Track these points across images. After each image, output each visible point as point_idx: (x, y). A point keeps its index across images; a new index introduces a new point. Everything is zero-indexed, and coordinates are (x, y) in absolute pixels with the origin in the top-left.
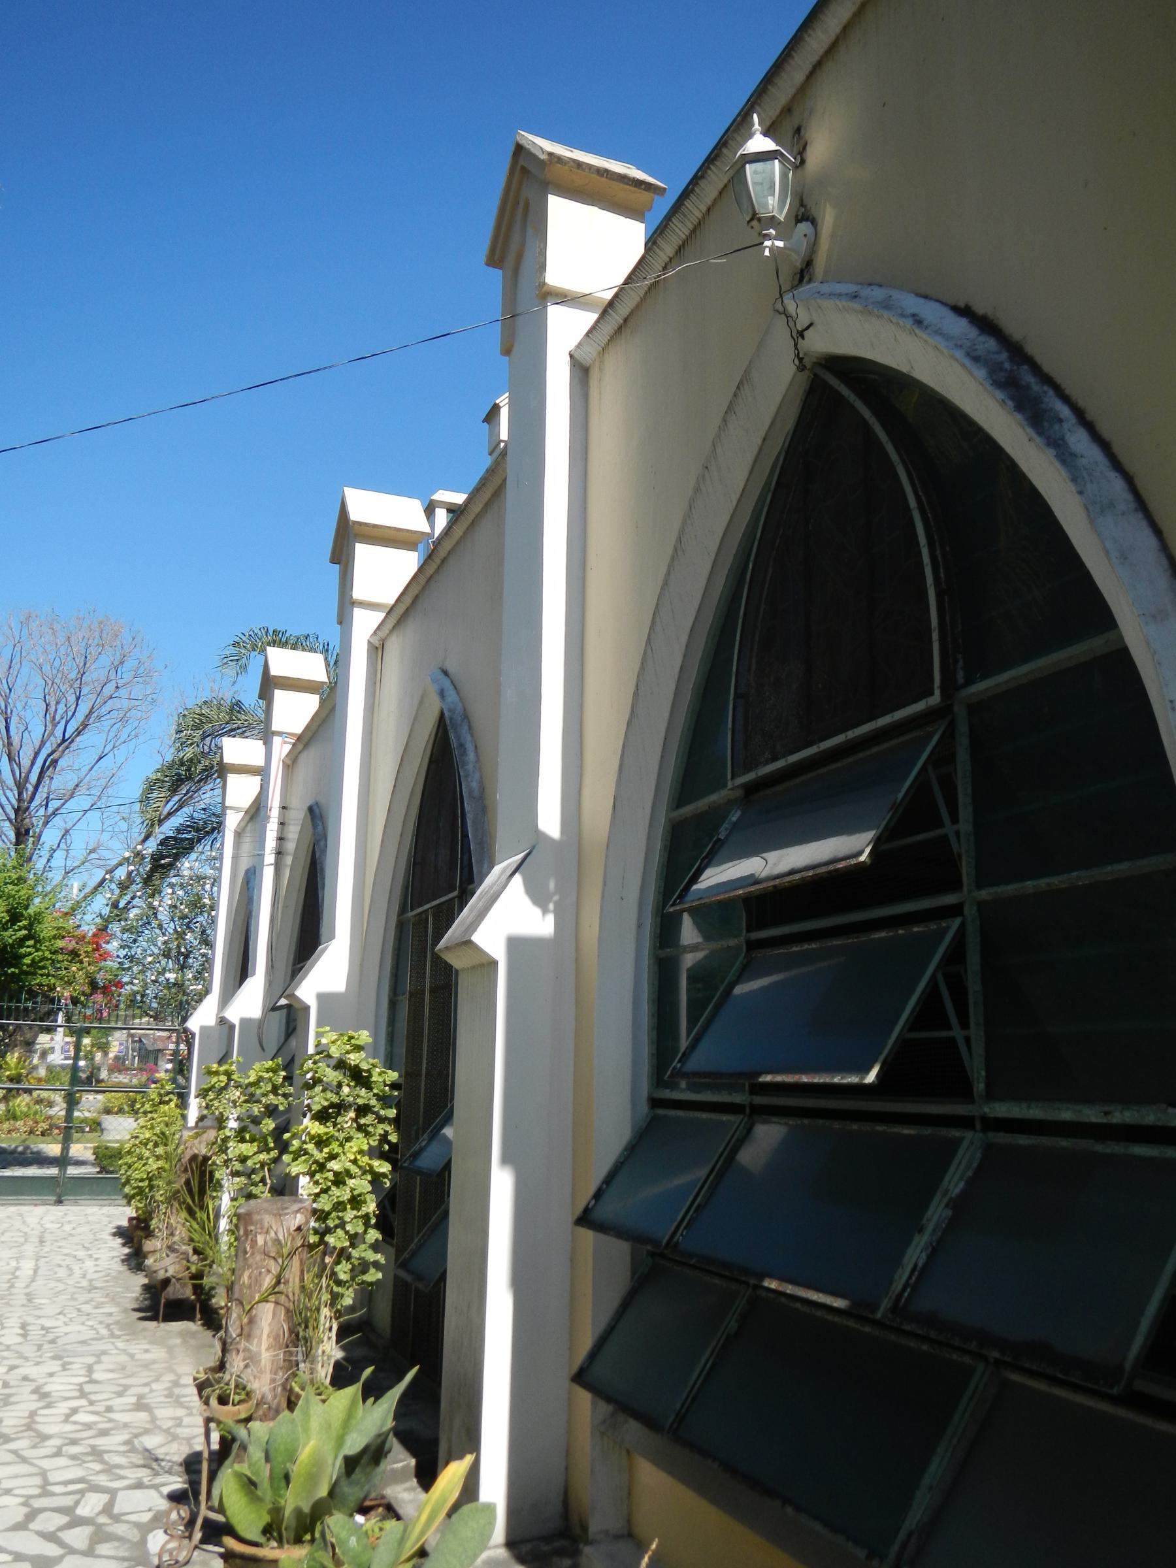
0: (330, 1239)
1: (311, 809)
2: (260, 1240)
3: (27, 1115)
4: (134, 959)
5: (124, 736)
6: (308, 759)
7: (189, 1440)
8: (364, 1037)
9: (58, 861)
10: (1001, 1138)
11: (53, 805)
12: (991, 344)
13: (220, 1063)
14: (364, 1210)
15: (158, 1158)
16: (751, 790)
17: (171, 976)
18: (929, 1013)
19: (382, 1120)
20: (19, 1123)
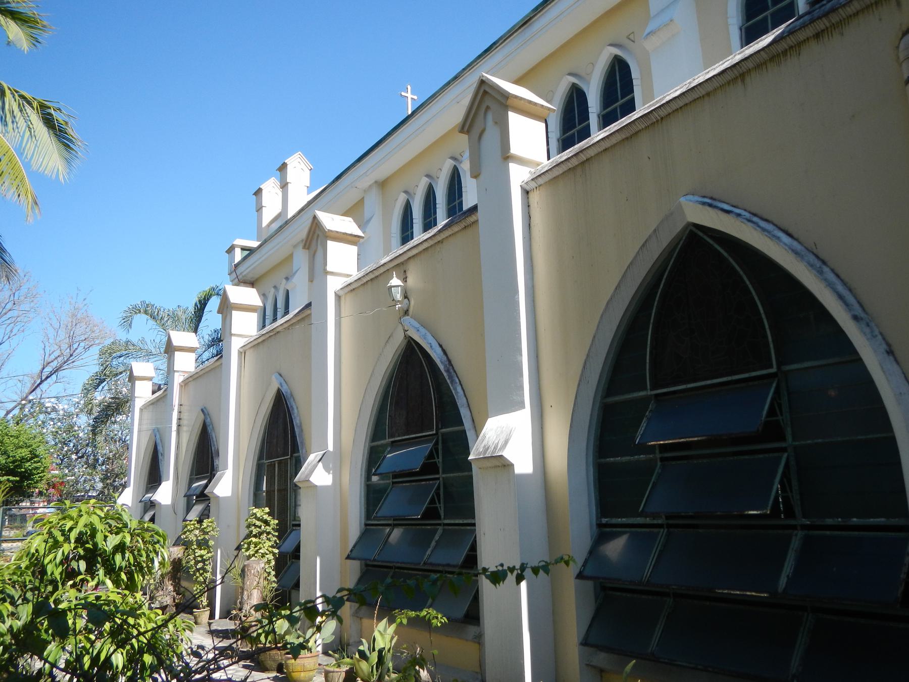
10: (446, 527)
12: (445, 358)
16: (393, 442)
18: (432, 501)
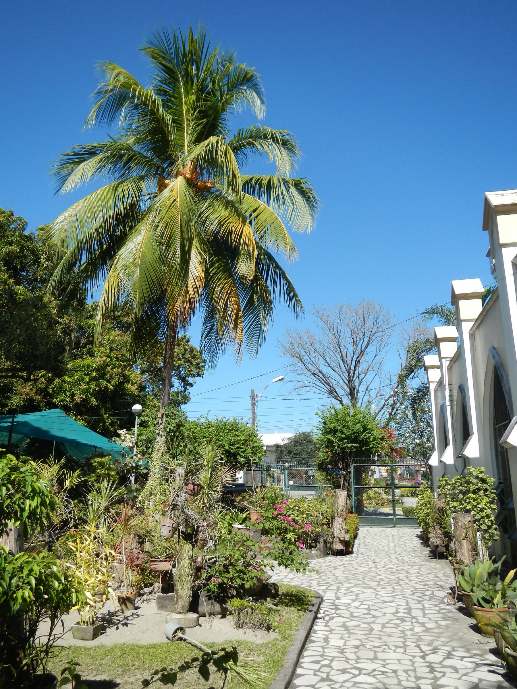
0: (482, 527)
1: (459, 387)
2: (460, 524)
3: (374, 498)
4: (404, 435)
5: (383, 346)
6: (456, 367)
7: (451, 584)
8: (483, 469)
9: (366, 399)
11: (361, 376)
13: (443, 477)
14: (491, 519)
15: (428, 509)
17: (418, 441)
19: (492, 493)
20: (373, 501)
